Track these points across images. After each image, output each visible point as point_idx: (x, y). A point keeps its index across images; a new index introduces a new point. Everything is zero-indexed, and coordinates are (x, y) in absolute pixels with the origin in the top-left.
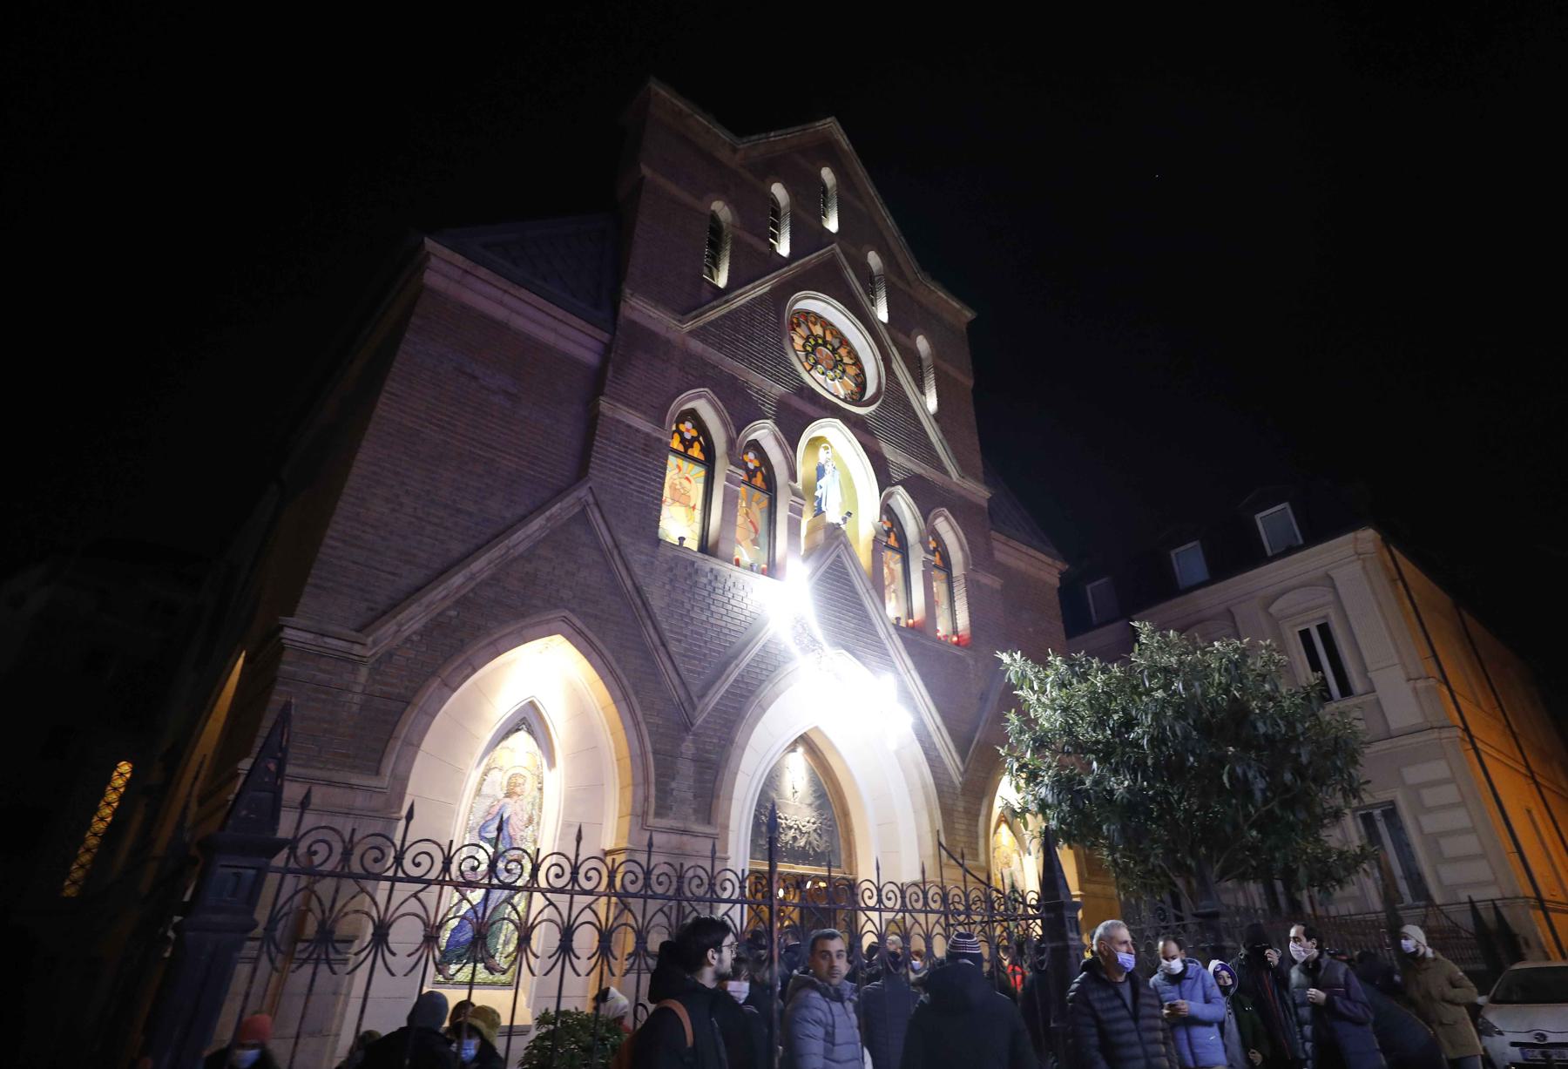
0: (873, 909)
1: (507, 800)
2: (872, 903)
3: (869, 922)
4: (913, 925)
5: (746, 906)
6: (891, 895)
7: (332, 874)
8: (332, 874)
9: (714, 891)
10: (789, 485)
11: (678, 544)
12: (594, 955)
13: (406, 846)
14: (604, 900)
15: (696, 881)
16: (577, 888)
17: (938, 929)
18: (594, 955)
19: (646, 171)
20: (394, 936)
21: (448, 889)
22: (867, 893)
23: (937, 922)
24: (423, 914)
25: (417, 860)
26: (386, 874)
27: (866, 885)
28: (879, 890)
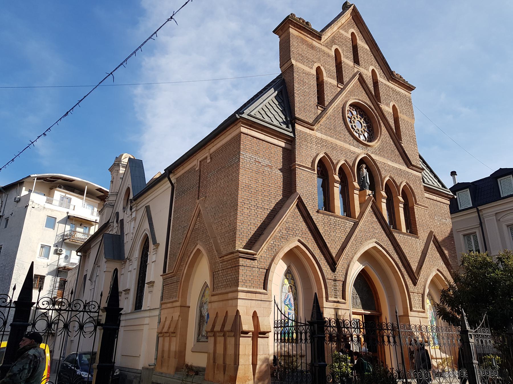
0: (386, 330)
1: (289, 293)
2: (385, 328)
3: (77, 316)
4: (333, 331)
5: (358, 329)
6: (424, 328)
7: (82, 311)
8: (82, 311)
9: (388, 328)
10: (376, 201)
11: (478, 207)
12: (78, 329)
13: (278, 310)
14: (357, 329)
15: (429, 328)
16: (352, 327)
17: (391, 335)
18: (78, 329)
19: (294, 62)
20: (71, 328)
21: (85, 313)
22: (384, 326)
23: (391, 333)
24: (78, 321)
25: (43, 303)
26: (7, 306)
27: (412, 325)
28: (387, 325)
